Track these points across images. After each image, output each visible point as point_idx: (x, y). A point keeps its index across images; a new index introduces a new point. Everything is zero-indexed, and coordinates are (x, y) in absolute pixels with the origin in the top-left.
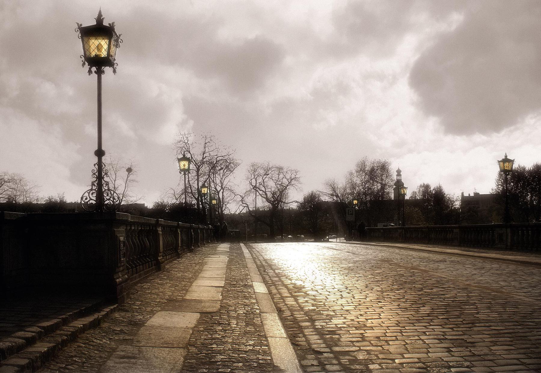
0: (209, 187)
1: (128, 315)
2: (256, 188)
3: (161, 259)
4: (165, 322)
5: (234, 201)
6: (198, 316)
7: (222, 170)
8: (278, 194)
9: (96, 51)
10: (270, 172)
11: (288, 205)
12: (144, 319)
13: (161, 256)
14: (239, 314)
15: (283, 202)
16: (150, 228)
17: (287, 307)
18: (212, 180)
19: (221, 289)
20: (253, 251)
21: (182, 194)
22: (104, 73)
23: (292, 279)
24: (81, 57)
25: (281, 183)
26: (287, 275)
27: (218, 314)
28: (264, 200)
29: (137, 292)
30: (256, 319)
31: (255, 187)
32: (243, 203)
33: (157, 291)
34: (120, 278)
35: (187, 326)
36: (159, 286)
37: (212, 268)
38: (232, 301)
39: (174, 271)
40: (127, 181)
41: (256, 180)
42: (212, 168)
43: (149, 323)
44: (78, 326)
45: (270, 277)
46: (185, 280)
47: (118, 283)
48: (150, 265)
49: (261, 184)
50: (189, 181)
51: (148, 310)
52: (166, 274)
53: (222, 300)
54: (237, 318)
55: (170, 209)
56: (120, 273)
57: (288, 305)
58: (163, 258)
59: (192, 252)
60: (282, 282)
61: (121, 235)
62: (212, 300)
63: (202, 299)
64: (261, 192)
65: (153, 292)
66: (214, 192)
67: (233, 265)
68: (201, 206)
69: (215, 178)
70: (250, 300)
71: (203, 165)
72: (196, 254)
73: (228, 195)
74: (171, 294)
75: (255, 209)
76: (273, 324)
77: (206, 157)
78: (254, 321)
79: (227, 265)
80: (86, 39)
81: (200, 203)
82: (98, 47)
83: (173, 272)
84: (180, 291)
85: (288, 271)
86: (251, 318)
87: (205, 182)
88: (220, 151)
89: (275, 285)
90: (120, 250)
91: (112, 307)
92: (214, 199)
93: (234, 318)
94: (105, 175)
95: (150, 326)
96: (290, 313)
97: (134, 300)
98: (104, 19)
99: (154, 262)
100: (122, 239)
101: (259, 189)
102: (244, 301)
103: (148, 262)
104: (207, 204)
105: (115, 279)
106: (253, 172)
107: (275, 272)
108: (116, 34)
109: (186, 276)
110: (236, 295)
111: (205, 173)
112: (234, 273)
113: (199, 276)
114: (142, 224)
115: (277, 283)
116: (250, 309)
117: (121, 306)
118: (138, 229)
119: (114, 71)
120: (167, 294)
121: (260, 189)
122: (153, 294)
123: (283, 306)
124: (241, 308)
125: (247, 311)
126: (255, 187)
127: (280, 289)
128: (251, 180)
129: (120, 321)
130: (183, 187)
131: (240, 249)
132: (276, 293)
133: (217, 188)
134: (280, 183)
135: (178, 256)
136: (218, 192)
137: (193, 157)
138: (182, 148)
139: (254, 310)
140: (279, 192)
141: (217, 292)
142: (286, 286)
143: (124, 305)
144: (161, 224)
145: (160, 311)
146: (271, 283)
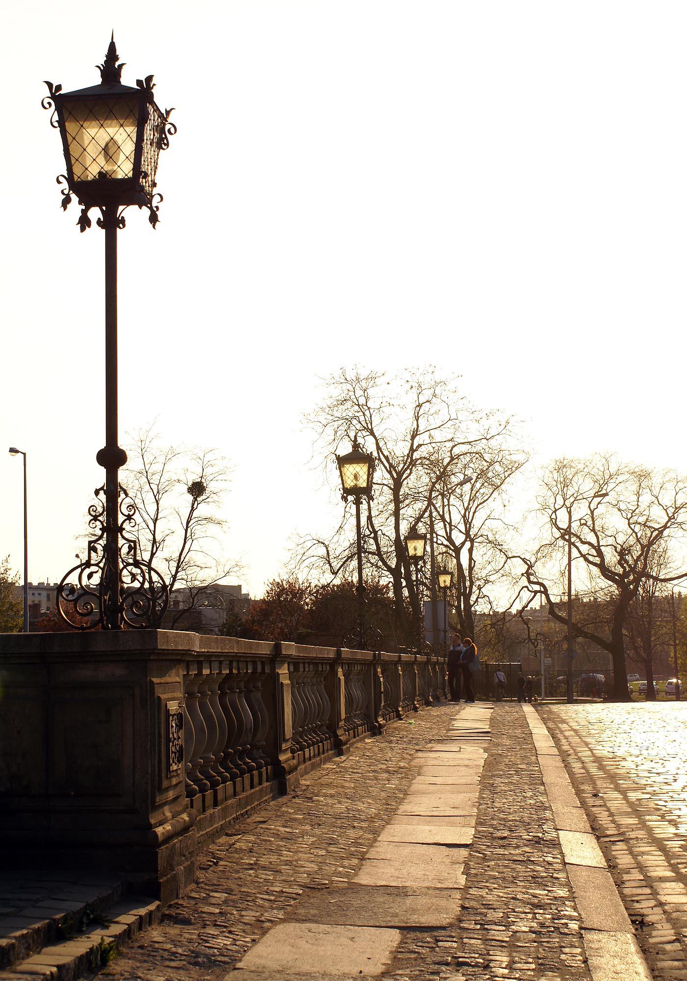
0: (429, 537)
1: (187, 936)
2: (570, 538)
3: (288, 760)
4: (296, 957)
5: (503, 575)
6: (394, 936)
7: (468, 484)
8: (636, 554)
9: (101, 160)
10: (611, 486)
11: (668, 585)
12: (234, 948)
13: (287, 749)
14: (518, 934)
15: (652, 577)
16: (255, 669)
17: (665, 912)
18: (438, 512)
19: (464, 852)
20: (559, 728)
21: (350, 558)
22: (124, 226)
23: (681, 823)
24: (59, 182)
25: (645, 518)
26: (664, 808)
27: (453, 934)
28: (596, 571)
29: (216, 864)
30: (567, 950)
31: (567, 534)
32: (530, 582)
33: (274, 858)
34: (165, 823)
35: (361, 972)
36: (281, 843)
37: (438, 787)
38: (495, 892)
39: (325, 795)
40: (191, 522)
41: (570, 513)
42: (439, 478)
43: (249, 960)
44: (43, 971)
45: (611, 815)
46: (356, 824)
47: (160, 838)
48: (256, 780)
49: (585, 524)
50: (370, 518)
51: (246, 919)
52: (302, 806)
53: (467, 888)
54: (511, 946)
55: (314, 603)
56: (166, 808)
57: (665, 904)
58: (293, 758)
59: (380, 733)
60: (650, 831)
61: (170, 695)
62: (438, 889)
63: (407, 884)
64: (585, 549)
65: (263, 861)
66: (444, 549)
67: (500, 776)
68: (406, 592)
69: (446, 509)
70: (550, 889)
71: (411, 470)
72: (391, 742)
73: (486, 558)
74: (316, 868)
75: (566, 598)
76: (619, 968)
77: (420, 446)
78: (563, 957)
79: (483, 777)
80: (71, 127)
81: (404, 584)
82: (106, 149)
83: (322, 799)
84: (342, 858)
85: (665, 797)
86: (553, 948)
87: (418, 520)
88: (463, 426)
89: (626, 841)
90: (168, 740)
91: (143, 911)
92: (446, 572)
93: (503, 946)
94: (128, 521)
95: (253, 969)
96: (673, 931)
97: (207, 887)
98: (124, 67)
99: (267, 769)
100: (173, 706)
101: (578, 537)
102: (531, 891)
103: (250, 770)
104: (424, 584)
105: (150, 827)
106: (559, 486)
107: (626, 798)
108: (157, 109)
109: (358, 810)
110: (508, 873)
111: (419, 493)
112: (504, 803)
113: (399, 812)
114: (233, 659)
115: (633, 835)
116: (550, 916)
117: (170, 906)
118: (220, 673)
119: (154, 219)
120: (302, 869)
121: (581, 539)
122: (264, 868)
123: (652, 908)
124: (523, 916)
125: (542, 925)
126: (567, 534)
127: (643, 853)
128: (555, 512)
129: (166, 954)
130: (350, 535)
131: (524, 724)
132: (629, 866)
133: (453, 537)
134: (642, 520)
135: (339, 748)
136: (457, 550)
137: (384, 448)
138: (349, 420)
139: (563, 921)
140: (639, 547)
141: (453, 863)
142: (660, 845)
143: (177, 904)
144: (289, 656)
145: (283, 921)
146: (616, 832)
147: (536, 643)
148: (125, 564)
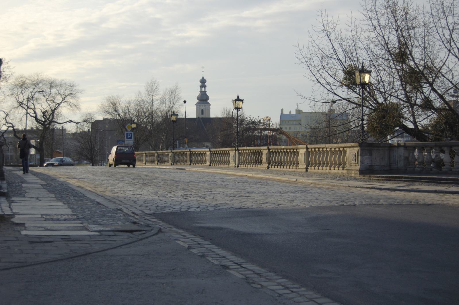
128: (18, 95)
147: (9, 146)
148: (439, 69)
